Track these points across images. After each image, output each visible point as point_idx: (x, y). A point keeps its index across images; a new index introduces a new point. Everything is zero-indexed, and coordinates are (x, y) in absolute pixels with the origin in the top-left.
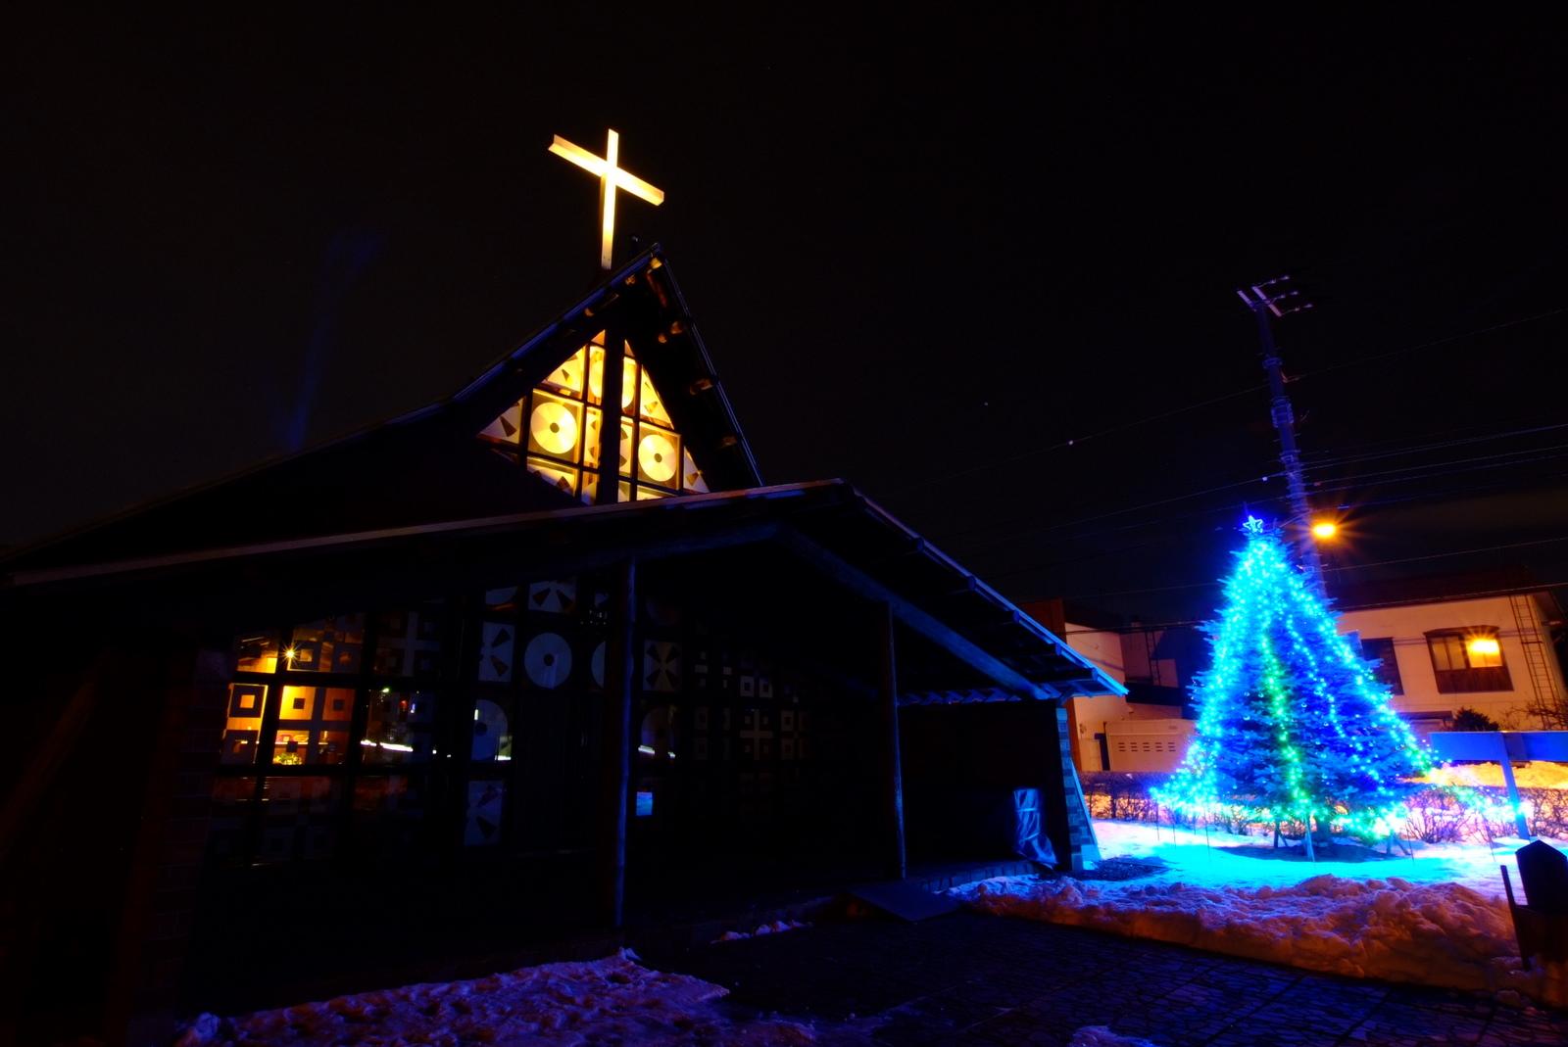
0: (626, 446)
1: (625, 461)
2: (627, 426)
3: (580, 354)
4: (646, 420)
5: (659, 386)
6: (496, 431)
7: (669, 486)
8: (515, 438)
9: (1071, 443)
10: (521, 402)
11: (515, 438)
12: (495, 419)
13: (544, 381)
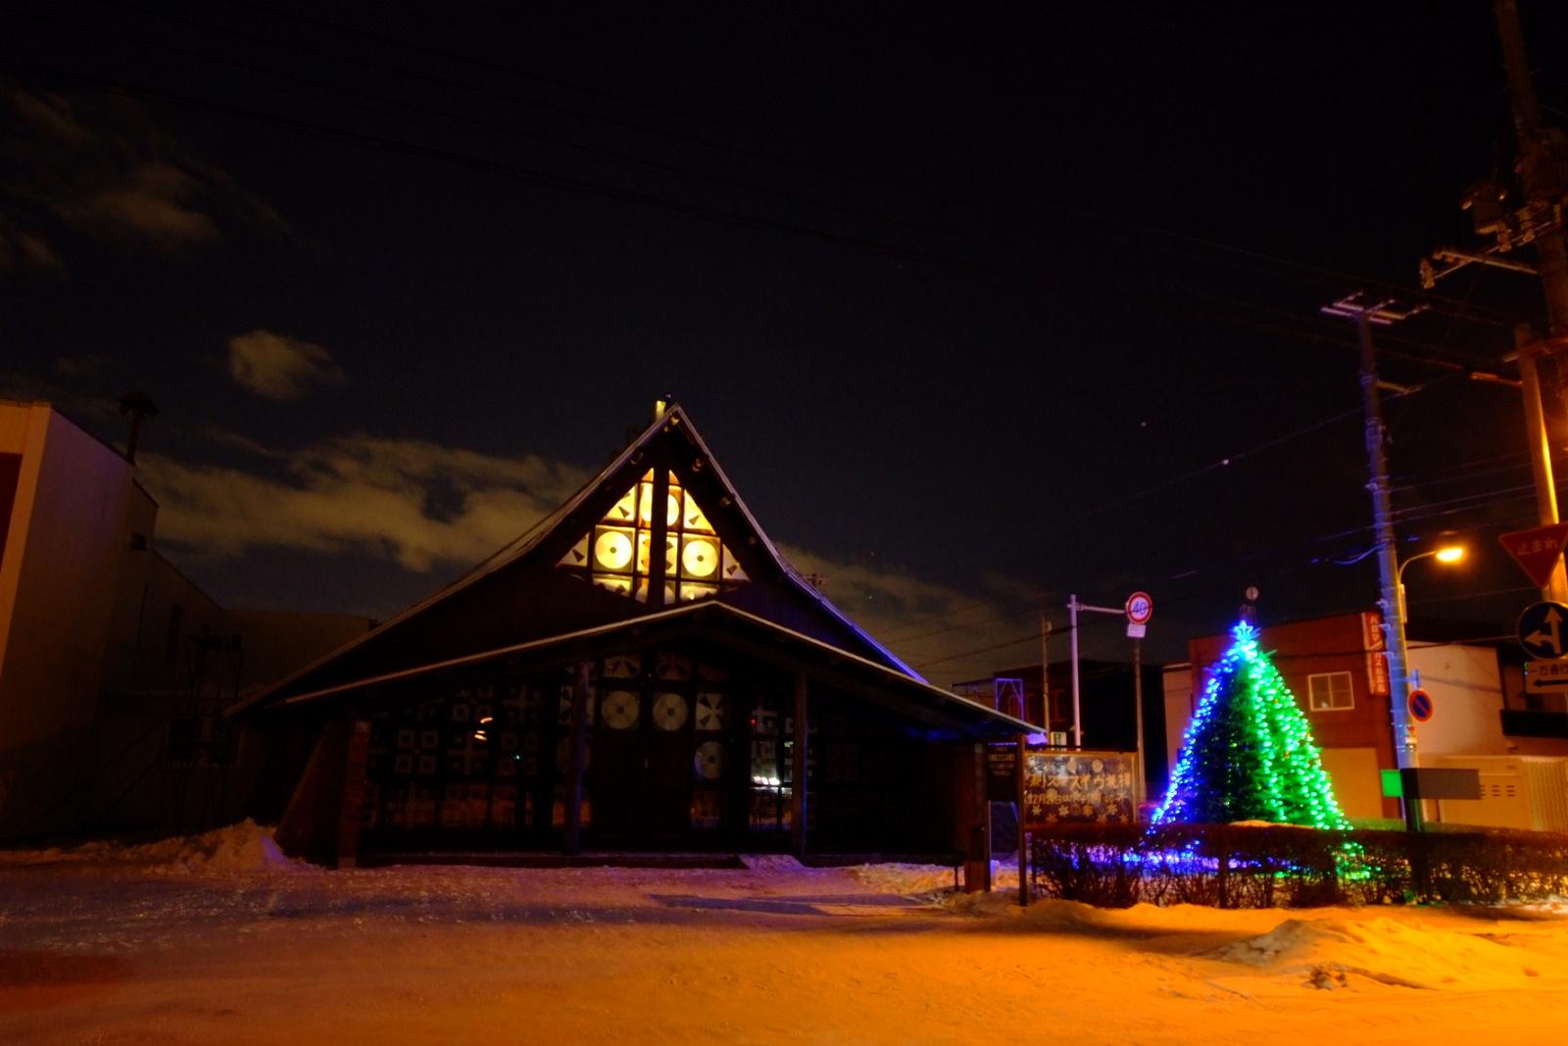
0: (671, 555)
1: (670, 565)
2: (672, 540)
3: (633, 491)
4: (689, 531)
5: (700, 502)
6: (570, 559)
7: (627, 571)
8: (584, 562)
9: (1226, 462)
10: (587, 536)
11: (584, 562)
12: (568, 551)
13: (605, 518)
